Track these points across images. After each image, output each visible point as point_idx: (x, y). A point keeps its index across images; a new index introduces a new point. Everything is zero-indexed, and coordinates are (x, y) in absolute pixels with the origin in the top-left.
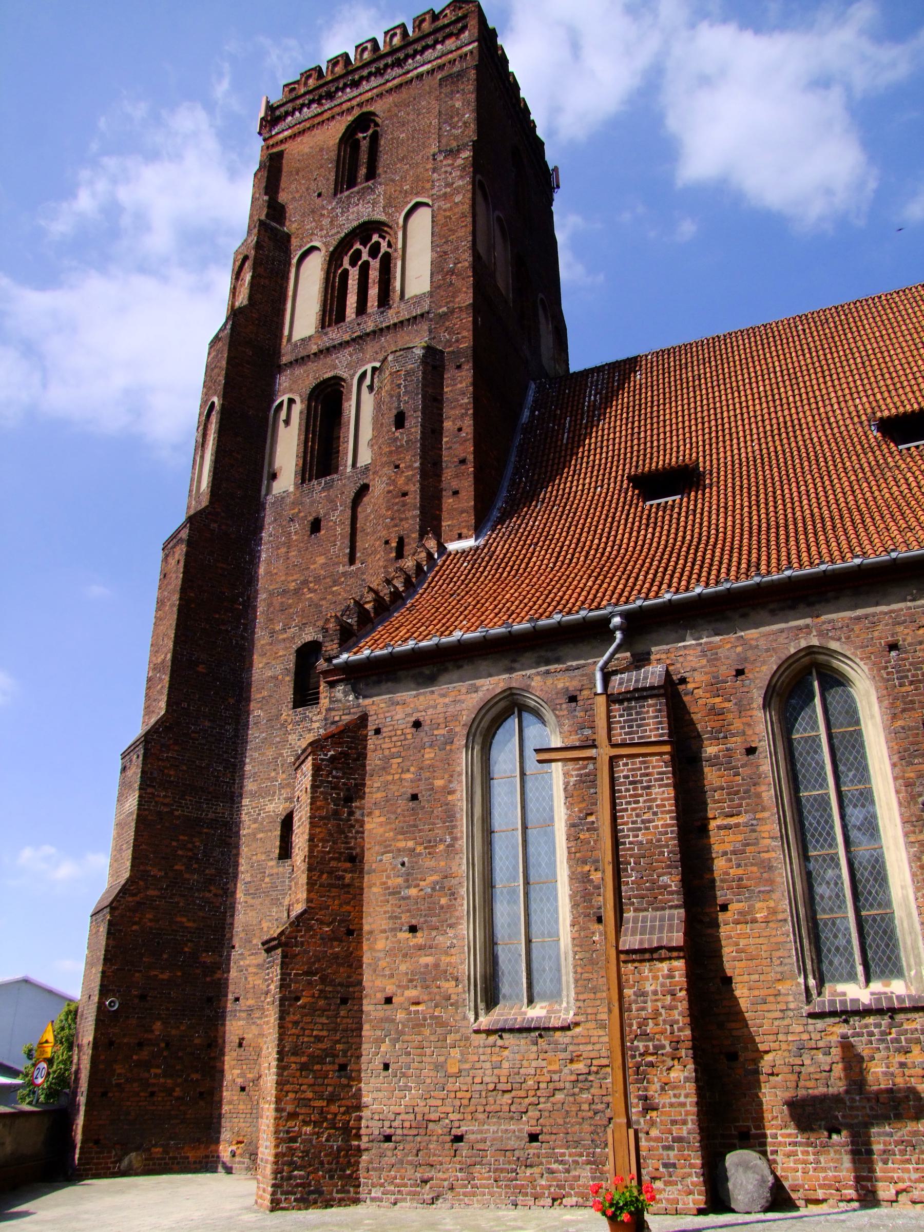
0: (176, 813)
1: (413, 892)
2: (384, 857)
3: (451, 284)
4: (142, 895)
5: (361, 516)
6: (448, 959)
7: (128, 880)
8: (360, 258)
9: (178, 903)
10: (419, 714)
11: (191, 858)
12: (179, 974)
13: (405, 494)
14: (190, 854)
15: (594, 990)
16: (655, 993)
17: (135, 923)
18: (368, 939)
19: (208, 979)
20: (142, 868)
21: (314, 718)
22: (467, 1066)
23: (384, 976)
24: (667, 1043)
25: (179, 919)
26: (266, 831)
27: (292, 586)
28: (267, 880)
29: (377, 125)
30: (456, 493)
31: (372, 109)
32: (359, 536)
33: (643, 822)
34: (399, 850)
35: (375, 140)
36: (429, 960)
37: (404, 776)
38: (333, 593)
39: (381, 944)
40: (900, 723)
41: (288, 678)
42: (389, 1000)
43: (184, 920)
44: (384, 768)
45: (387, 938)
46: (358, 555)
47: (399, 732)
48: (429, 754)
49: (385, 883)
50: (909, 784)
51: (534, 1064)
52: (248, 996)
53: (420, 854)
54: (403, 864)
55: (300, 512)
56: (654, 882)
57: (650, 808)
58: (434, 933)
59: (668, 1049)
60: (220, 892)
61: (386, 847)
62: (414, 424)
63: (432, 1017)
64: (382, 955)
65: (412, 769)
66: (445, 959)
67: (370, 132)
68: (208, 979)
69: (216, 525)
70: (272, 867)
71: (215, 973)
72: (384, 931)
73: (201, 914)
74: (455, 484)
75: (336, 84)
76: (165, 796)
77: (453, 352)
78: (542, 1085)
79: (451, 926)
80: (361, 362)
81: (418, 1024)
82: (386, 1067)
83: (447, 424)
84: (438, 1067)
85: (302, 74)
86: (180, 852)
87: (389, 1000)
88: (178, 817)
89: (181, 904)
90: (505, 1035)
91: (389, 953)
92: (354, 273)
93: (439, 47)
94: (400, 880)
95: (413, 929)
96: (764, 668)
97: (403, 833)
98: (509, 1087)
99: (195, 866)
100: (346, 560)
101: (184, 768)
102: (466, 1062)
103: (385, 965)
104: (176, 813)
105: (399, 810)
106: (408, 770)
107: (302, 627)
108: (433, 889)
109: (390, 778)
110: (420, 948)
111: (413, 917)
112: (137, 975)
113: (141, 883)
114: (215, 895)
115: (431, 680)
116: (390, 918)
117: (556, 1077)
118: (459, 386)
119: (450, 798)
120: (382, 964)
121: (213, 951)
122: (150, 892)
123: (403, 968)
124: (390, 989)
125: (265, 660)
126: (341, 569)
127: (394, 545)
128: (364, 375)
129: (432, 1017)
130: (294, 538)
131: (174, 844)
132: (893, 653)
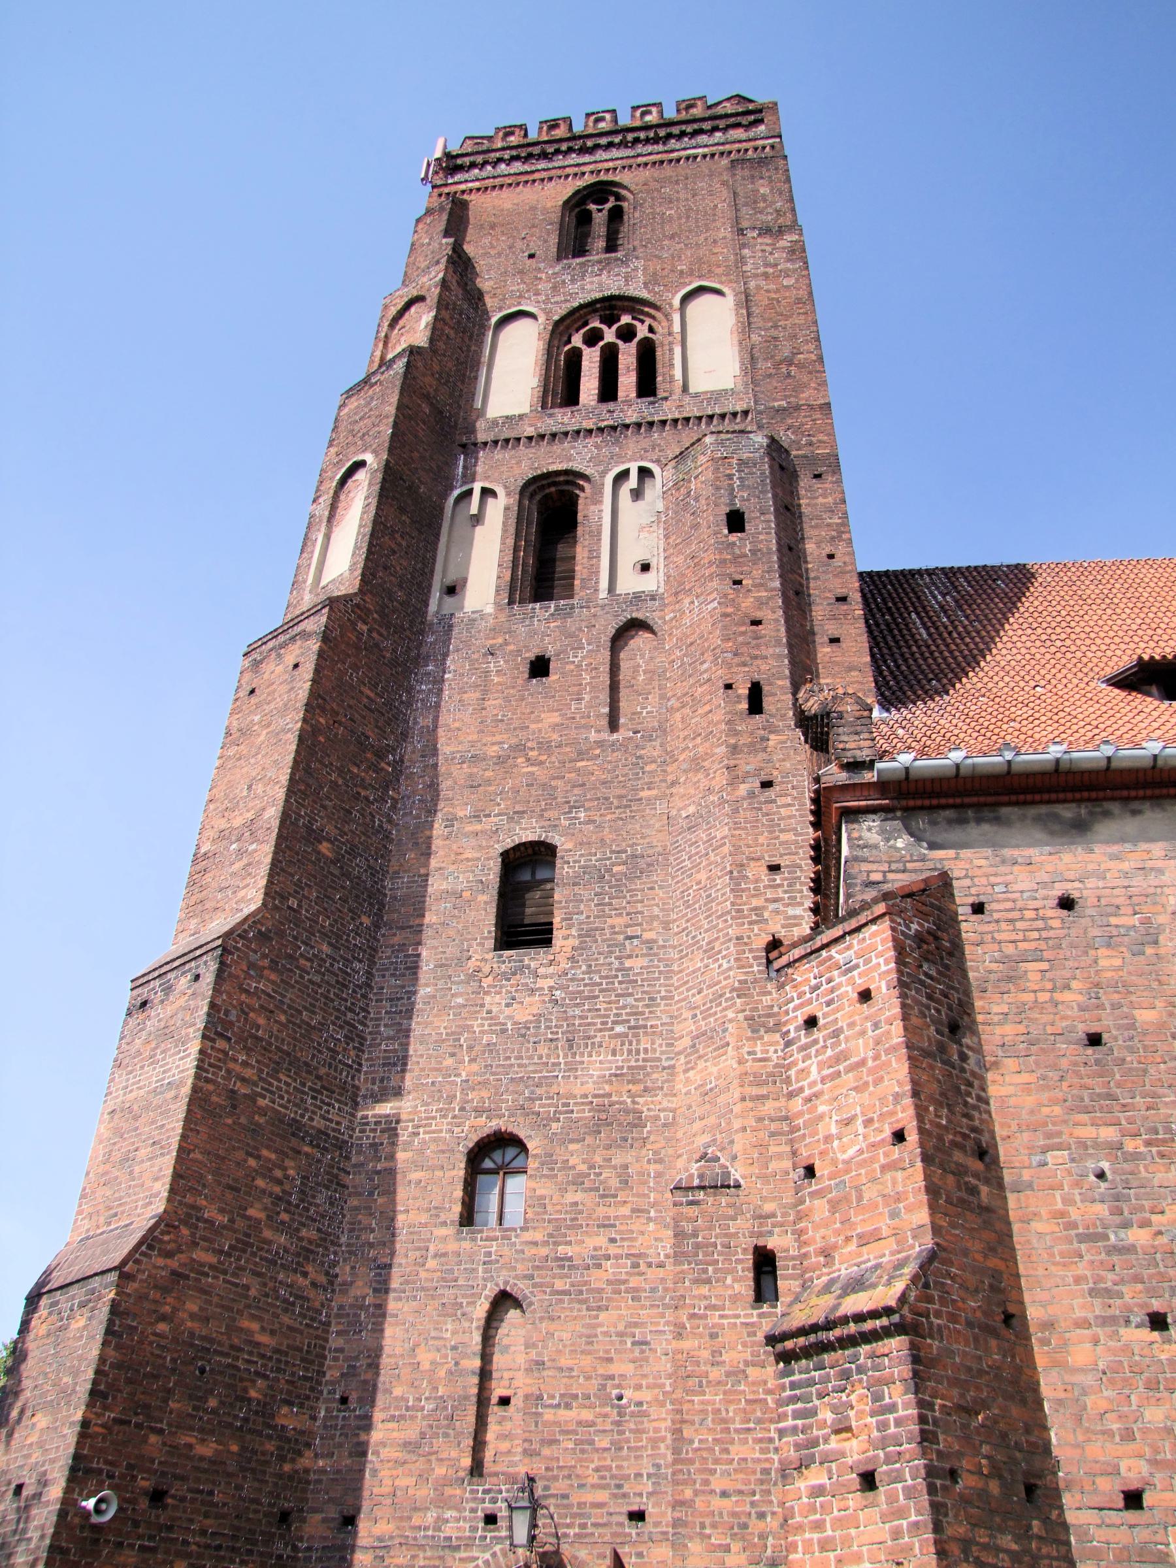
0: (262, 1102)
1: (1138, 1236)
2: (1049, 1157)
3: (789, 375)
4: (182, 1257)
5: (625, 666)
7: (161, 1219)
8: (602, 339)
9: (247, 1288)
10: (1069, 886)
11: (279, 1199)
12: (235, 1448)
13: (756, 623)
14: (277, 1189)
17: (163, 1318)
18: (1045, 1342)
19: (287, 1467)
20: (189, 1199)
21: (541, 971)
23: (1109, 1433)
25: (246, 1323)
26: (432, 1169)
27: (493, 751)
28: (431, 1263)
29: (619, 197)
30: (835, 641)
31: (617, 179)
32: (623, 693)
35: (616, 215)
37: (1058, 996)
39: (1081, 1354)
41: (483, 898)
42: (1133, 1499)
43: (255, 1326)
44: (1009, 979)
45: (1096, 1341)
46: (622, 721)
48: (1108, 961)
49: (1062, 1214)
52: (378, 1512)
54: (1101, 1175)
55: (506, 643)
60: (323, 1279)
61: (1049, 1136)
62: (763, 529)
64: (1089, 1380)
65: (1074, 984)
67: (609, 205)
68: (287, 1467)
69: (365, 628)
70: (444, 1239)
71: (300, 1454)
72: (1084, 1324)
73: (286, 1319)
74: (832, 629)
75: (556, 146)
76: (245, 1064)
77: (805, 457)
80: (621, 458)
83: (810, 547)
85: (498, 129)
86: (260, 1183)
88: (263, 1112)
89: (253, 1292)
92: (591, 360)
93: (718, 134)
94: (1102, 1210)
99: (285, 1216)
100: (604, 722)
101: (283, 1018)
103: (1103, 1405)
104: (262, 1102)
106: (1067, 987)
107: (516, 816)
109: (1028, 997)
111: (1153, 1293)
112: (153, 1439)
113: (185, 1231)
114: (314, 1284)
115: (1080, 828)
116: (1093, 1292)
121: (301, 1406)
122: (199, 1255)
124: (1133, 1471)
126: (593, 736)
128: (625, 474)
130: (496, 679)
131: (252, 1162)
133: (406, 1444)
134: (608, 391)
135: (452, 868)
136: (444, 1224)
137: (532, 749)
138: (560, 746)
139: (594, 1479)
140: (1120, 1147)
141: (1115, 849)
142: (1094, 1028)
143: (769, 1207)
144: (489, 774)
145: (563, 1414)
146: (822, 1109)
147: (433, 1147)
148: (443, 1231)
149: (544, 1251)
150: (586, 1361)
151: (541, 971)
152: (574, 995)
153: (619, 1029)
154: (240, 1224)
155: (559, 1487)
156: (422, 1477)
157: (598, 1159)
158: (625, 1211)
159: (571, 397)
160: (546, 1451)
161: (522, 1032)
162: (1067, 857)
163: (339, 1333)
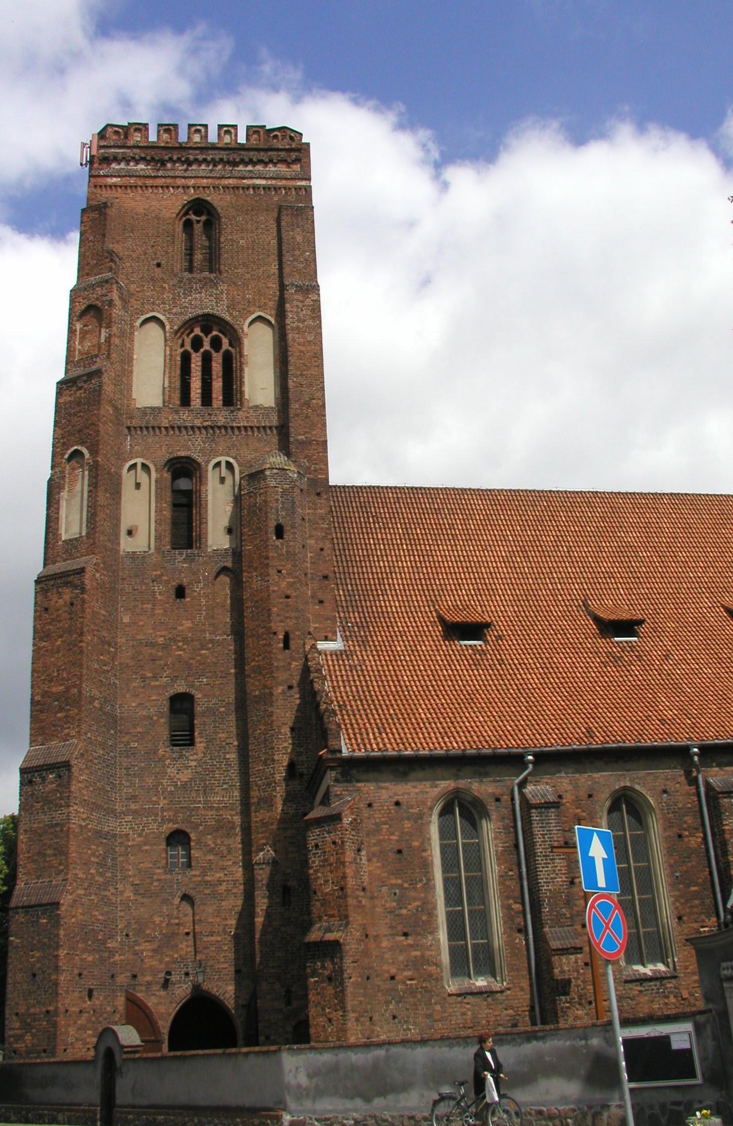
1: (404, 911)
6: (430, 953)
8: (202, 346)
15: (518, 970)
16: (569, 971)
17: (73, 917)
19: (112, 960)
22: (446, 1015)
24: (576, 997)
33: (551, 878)
34: (392, 885)
36: (418, 953)
38: (201, 655)
40: (667, 834)
41: (162, 720)
42: (393, 978)
47: (385, 808)
48: (407, 824)
50: (671, 866)
51: (486, 1011)
53: (406, 888)
54: (395, 894)
56: (557, 912)
57: (554, 871)
58: (419, 937)
59: (577, 999)
60: (114, 891)
63: (422, 987)
64: (386, 950)
65: (396, 833)
66: (428, 953)
70: (159, 874)
72: (386, 935)
78: (491, 1023)
79: (430, 933)
81: (412, 992)
82: (394, 1017)
84: (429, 1016)
87: (393, 978)
90: (468, 997)
91: (392, 949)
94: (394, 904)
95: (406, 934)
96: (603, 796)
97: (393, 874)
98: (472, 1025)
102: (445, 1012)
104: (90, 826)
105: (390, 860)
107: (174, 679)
108: (417, 910)
110: (411, 946)
113: (74, 884)
117: (498, 1018)
118: (319, 511)
119: (424, 854)
120: (387, 956)
123: (401, 958)
124: (393, 971)
125: (138, 701)
127: (281, 637)
129: (422, 987)
131: (89, 852)
132: (665, 795)
133: (153, 950)
134: (207, 399)
135: (147, 704)
136: (159, 868)
137: (179, 641)
138: (192, 641)
139: (223, 960)
140: (402, 885)
141: (414, 784)
142: (400, 848)
143: (288, 871)
144: (160, 654)
145: (211, 938)
146: (319, 875)
147: (151, 836)
148: (158, 871)
149: (199, 879)
150: (218, 919)
151: (191, 758)
152: (205, 770)
153: (225, 786)
154: (89, 877)
155: (210, 963)
156: (161, 961)
157: (219, 842)
158: (230, 863)
159: (185, 400)
160: (205, 951)
161: (185, 786)
162: (400, 787)
163: (121, 911)
